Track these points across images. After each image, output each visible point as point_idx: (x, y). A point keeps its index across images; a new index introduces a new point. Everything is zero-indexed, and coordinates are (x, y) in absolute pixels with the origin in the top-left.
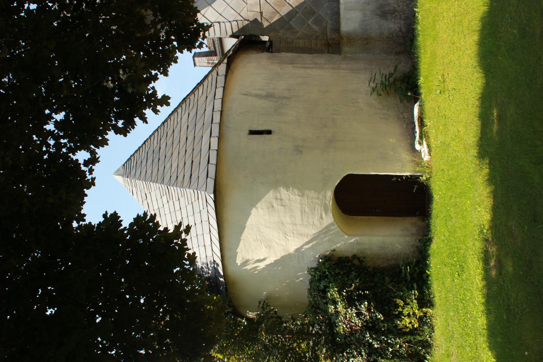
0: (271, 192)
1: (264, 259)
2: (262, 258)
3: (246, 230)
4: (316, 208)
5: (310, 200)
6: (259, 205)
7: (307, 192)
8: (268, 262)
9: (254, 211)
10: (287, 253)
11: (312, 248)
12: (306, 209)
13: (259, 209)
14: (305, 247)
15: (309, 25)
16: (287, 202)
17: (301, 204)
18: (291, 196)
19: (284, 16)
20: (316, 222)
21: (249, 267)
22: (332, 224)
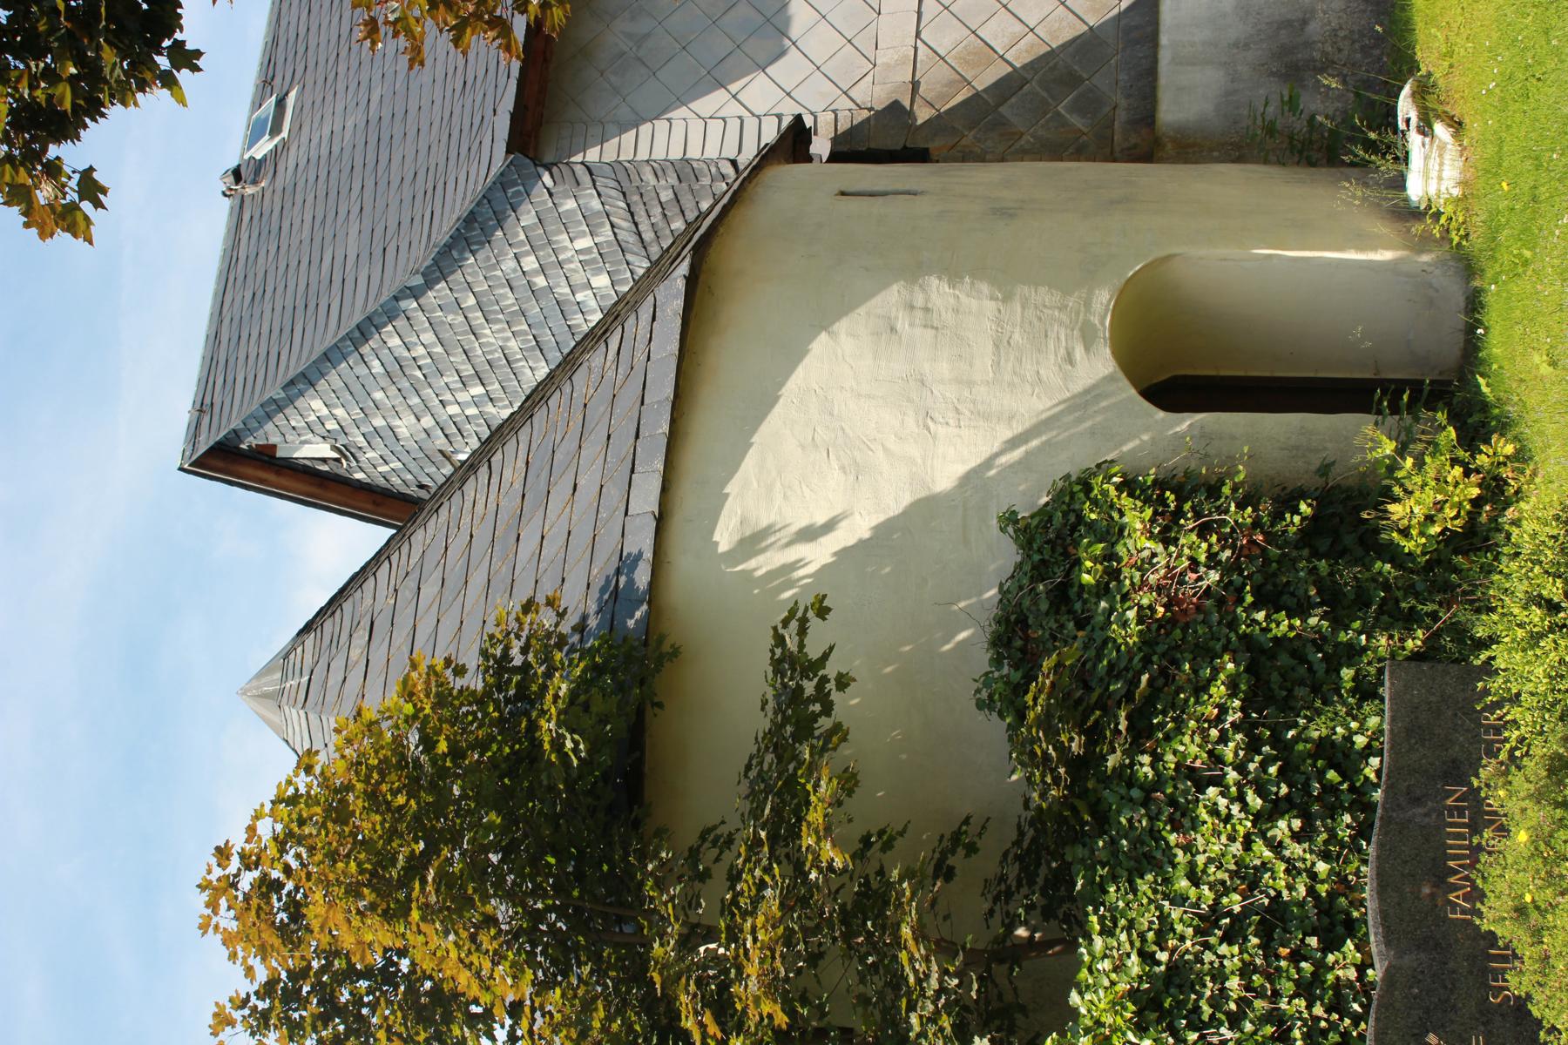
0: (895, 287)
1: (829, 526)
2: (820, 519)
3: (778, 410)
4: (1053, 335)
5: (1030, 313)
6: (842, 326)
7: (1022, 290)
8: (843, 537)
9: (820, 345)
10: (923, 494)
11: (1024, 464)
12: (1017, 336)
13: (843, 337)
14: (1003, 460)
15: (1059, 114)
16: (949, 317)
17: (999, 322)
18: (963, 297)
19: (985, 90)
20: (1049, 371)
21: (762, 564)
22: (1110, 379)
